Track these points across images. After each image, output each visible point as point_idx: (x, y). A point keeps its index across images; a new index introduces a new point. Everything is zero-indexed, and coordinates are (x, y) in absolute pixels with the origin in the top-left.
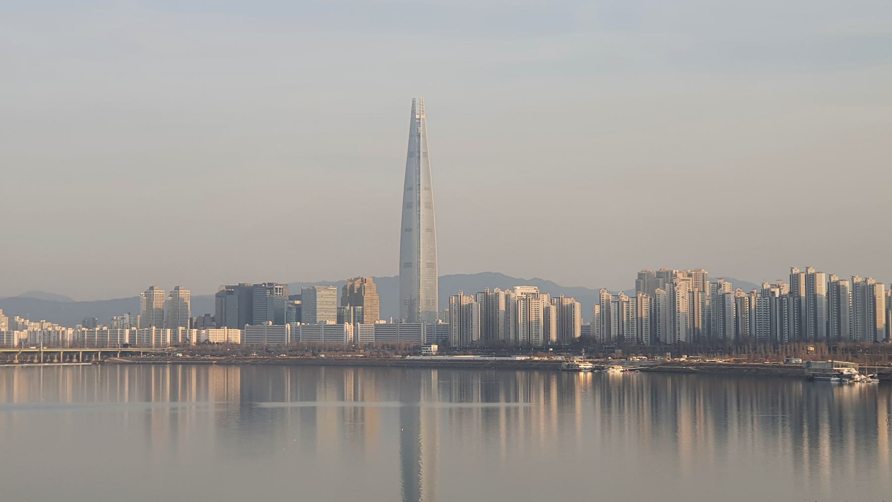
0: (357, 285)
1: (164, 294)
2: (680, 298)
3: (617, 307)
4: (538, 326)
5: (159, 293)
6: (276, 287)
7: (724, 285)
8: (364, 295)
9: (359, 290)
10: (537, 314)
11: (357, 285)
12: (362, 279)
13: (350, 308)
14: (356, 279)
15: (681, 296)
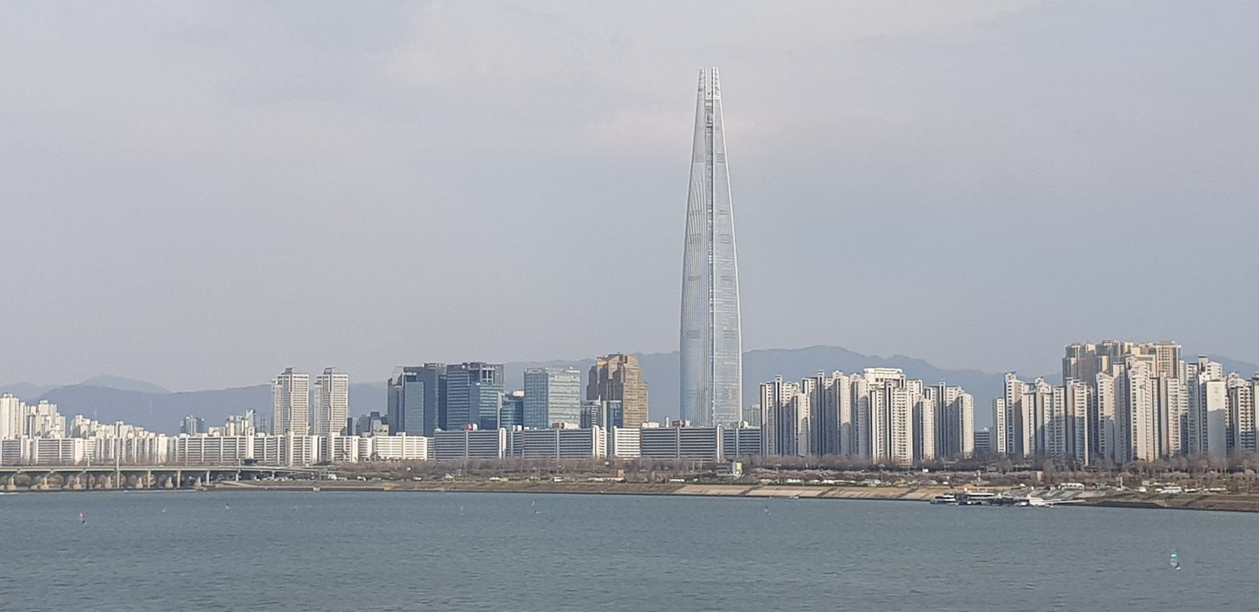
0: (613, 367)
1: (347, 379)
2: (1138, 391)
3: (1032, 402)
4: (904, 433)
5: (340, 379)
6: (484, 369)
7: (1102, 383)
8: (625, 382)
9: (617, 374)
10: (902, 413)
11: (613, 367)
12: (621, 357)
13: (602, 403)
14: (611, 356)
15: (1138, 385)
